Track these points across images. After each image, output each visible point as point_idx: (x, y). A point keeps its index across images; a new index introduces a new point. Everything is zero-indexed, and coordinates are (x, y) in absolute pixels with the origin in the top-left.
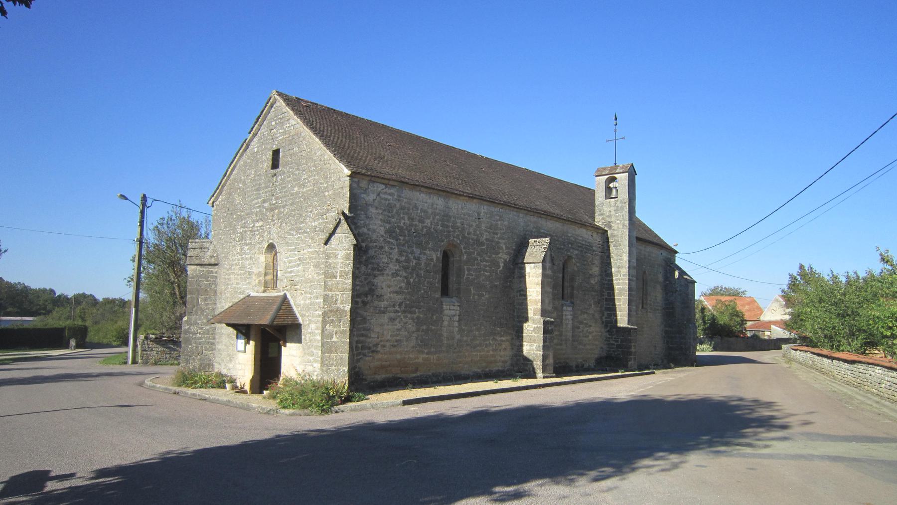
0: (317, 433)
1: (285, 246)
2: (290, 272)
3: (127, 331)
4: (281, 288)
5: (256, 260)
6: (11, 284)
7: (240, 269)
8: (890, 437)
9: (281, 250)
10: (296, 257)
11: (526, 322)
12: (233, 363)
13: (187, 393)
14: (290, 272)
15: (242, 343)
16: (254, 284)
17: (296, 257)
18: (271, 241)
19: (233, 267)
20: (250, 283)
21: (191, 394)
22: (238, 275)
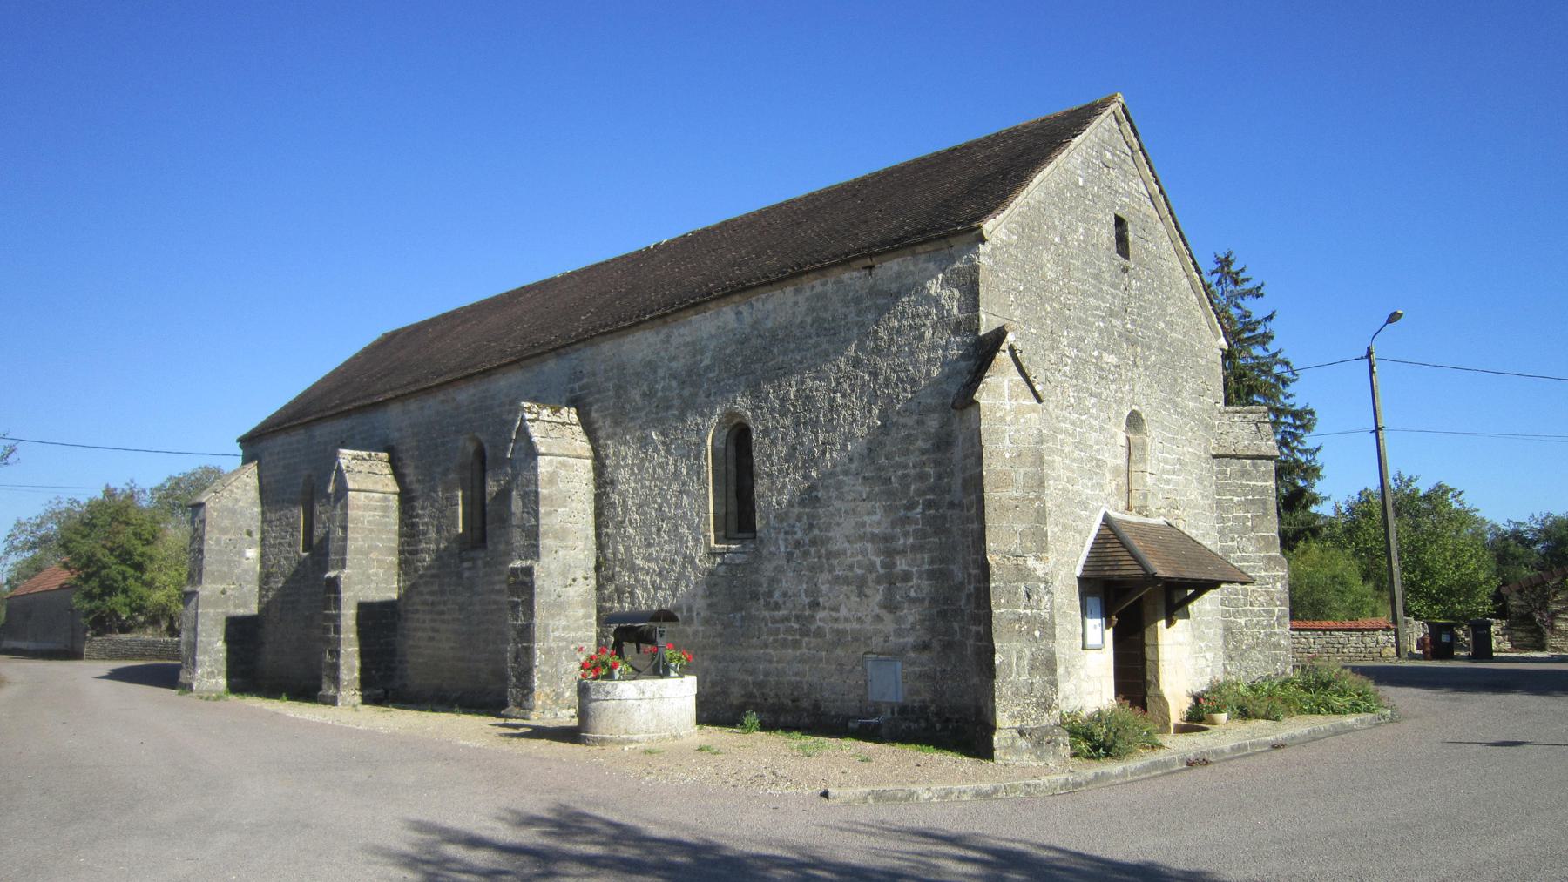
0: (1051, 854)
1: (1157, 428)
2: (1168, 482)
3: (751, 217)
4: (1154, 510)
5: (1112, 437)
6: (101, 503)
7: (1077, 445)
8: (572, 838)
9: (1154, 433)
10: (1174, 456)
11: (1131, 703)
12: (1073, 680)
13: (1223, 751)
14: (1168, 482)
15: (1095, 627)
16: (1108, 490)
17: (1174, 456)
18: (1135, 408)
19: (1059, 437)
20: (1100, 486)
21: (1232, 749)
22: (1073, 460)
